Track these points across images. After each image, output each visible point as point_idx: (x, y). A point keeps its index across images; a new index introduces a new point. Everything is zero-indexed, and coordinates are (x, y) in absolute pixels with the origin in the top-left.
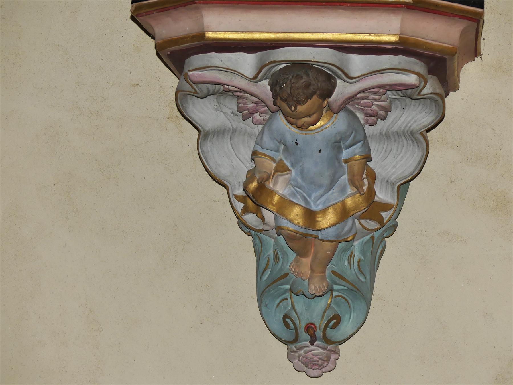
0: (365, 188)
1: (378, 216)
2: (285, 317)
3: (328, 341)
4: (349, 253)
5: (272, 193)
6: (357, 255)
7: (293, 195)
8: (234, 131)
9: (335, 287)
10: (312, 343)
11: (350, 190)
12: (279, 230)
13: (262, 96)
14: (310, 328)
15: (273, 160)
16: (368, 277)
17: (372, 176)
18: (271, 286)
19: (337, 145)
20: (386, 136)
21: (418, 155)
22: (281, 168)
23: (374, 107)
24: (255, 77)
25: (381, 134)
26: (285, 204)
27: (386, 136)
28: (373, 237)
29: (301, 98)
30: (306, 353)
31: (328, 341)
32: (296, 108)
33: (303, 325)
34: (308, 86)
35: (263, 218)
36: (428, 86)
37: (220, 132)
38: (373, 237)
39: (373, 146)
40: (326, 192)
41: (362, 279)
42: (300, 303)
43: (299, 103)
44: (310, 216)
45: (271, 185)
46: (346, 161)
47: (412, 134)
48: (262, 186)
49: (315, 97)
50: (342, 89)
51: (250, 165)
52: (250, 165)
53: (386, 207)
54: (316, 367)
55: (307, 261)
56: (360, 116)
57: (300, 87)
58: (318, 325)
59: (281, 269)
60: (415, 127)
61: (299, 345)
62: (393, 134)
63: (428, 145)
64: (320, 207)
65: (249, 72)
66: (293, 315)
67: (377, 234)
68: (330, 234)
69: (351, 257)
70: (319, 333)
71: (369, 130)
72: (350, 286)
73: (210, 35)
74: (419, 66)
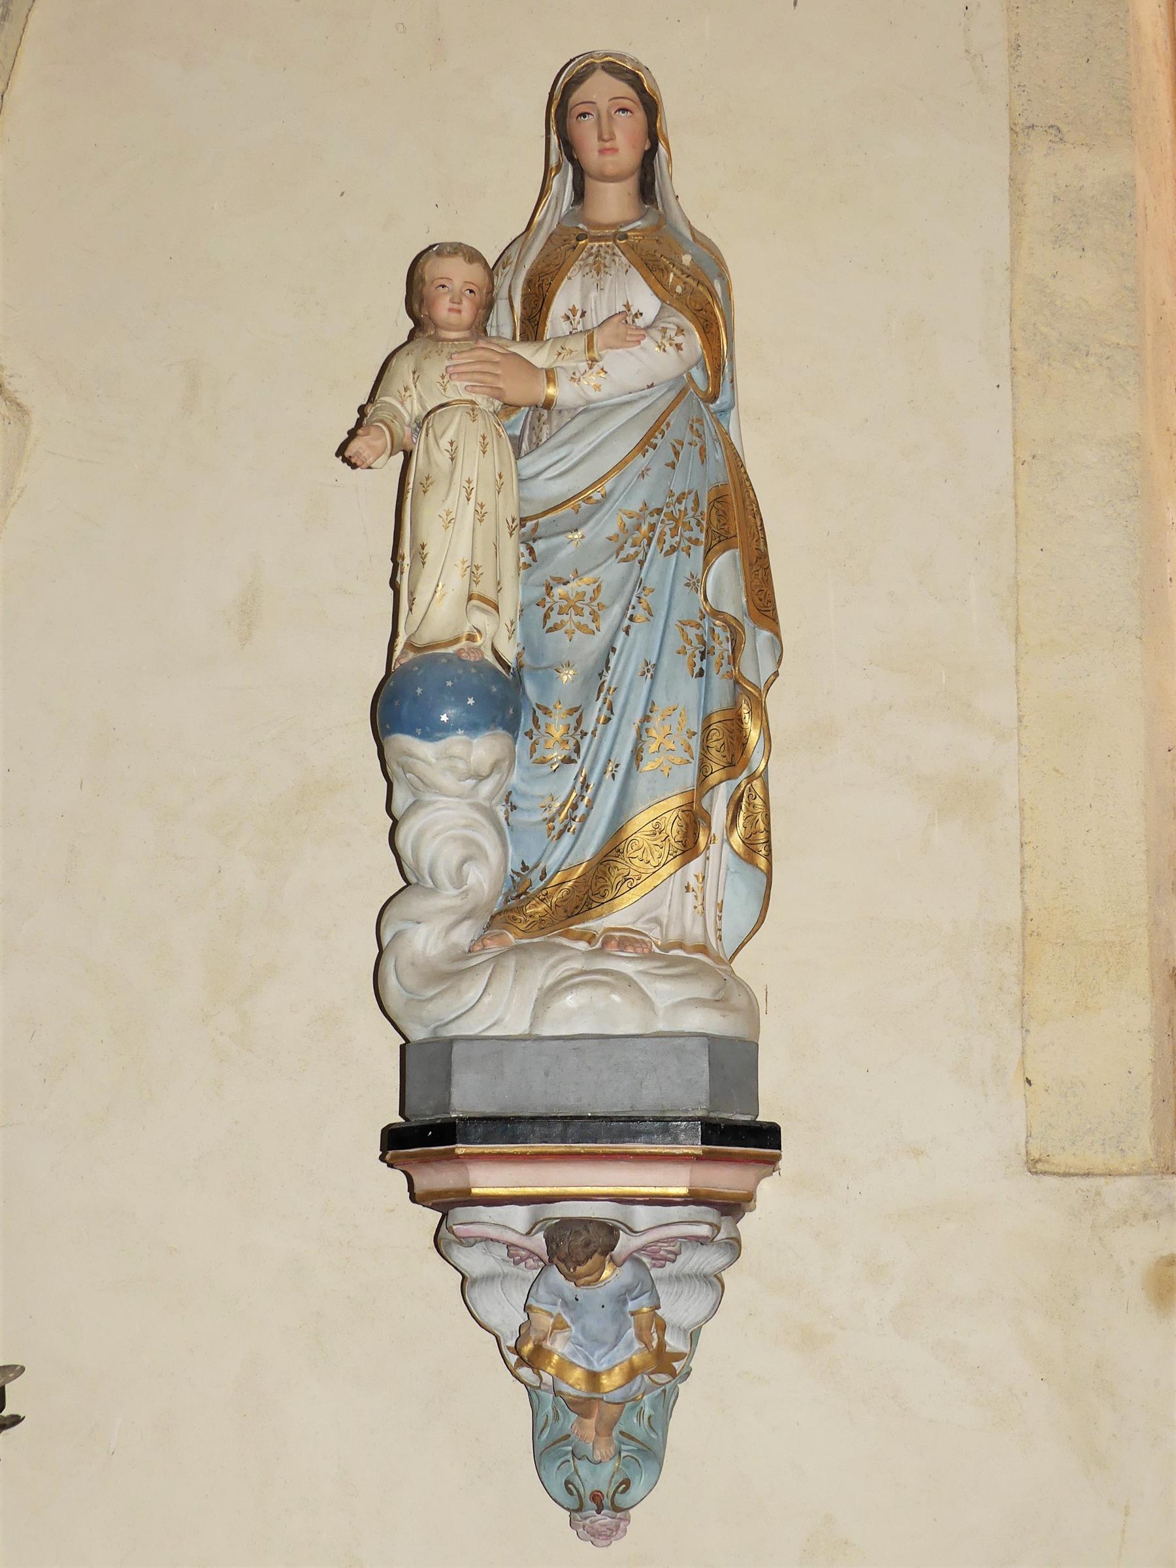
0: (654, 1344)
1: (665, 1364)
2: (567, 1483)
3: (616, 1509)
4: (638, 1409)
5: (550, 1353)
6: (648, 1411)
7: (574, 1354)
8: (505, 1276)
9: (623, 1447)
10: (599, 1513)
11: (637, 1345)
12: (557, 1393)
13: (537, 1251)
14: (596, 1497)
15: (550, 1315)
16: (660, 1434)
17: (662, 1327)
18: (550, 1449)
19: (621, 1299)
20: (677, 1278)
21: (712, 1297)
22: (559, 1326)
23: (662, 1252)
24: (528, 1233)
25: (670, 1276)
26: (565, 1365)
27: (677, 1278)
28: (664, 1391)
29: (582, 1257)
30: (592, 1522)
31: (616, 1509)
32: (575, 1269)
33: (588, 1493)
34: (587, 1244)
35: (541, 1378)
36: (722, 1230)
37: (489, 1278)
38: (664, 1391)
39: (661, 1289)
40: (610, 1350)
41: (653, 1436)
42: (584, 1468)
43: (579, 1263)
44: (593, 1378)
45: (547, 1344)
46: (633, 1314)
47: (705, 1276)
48: (538, 1348)
49: (596, 1256)
50: (625, 1243)
51: (522, 1318)
52: (522, 1318)
53: (679, 1356)
54: (601, 1537)
55: (591, 1423)
56: (645, 1260)
57: (577, 1245)
58: (605, 1494)
59: (561, 1429)
60: (708, 1269)
61: (584, 1514)
62: (684, 1276)
63: (723, 1286)
64: (605, 1367)
65: (522, 1227)
66: (577, 1482)
67: (668, 1387)
68: (618, 1395)
69: (640, 1414)
70: (607, 1502)
71: (654, 1272)
72: (640, 1446)
73: (475, 1191)
74: (710, 1214)
